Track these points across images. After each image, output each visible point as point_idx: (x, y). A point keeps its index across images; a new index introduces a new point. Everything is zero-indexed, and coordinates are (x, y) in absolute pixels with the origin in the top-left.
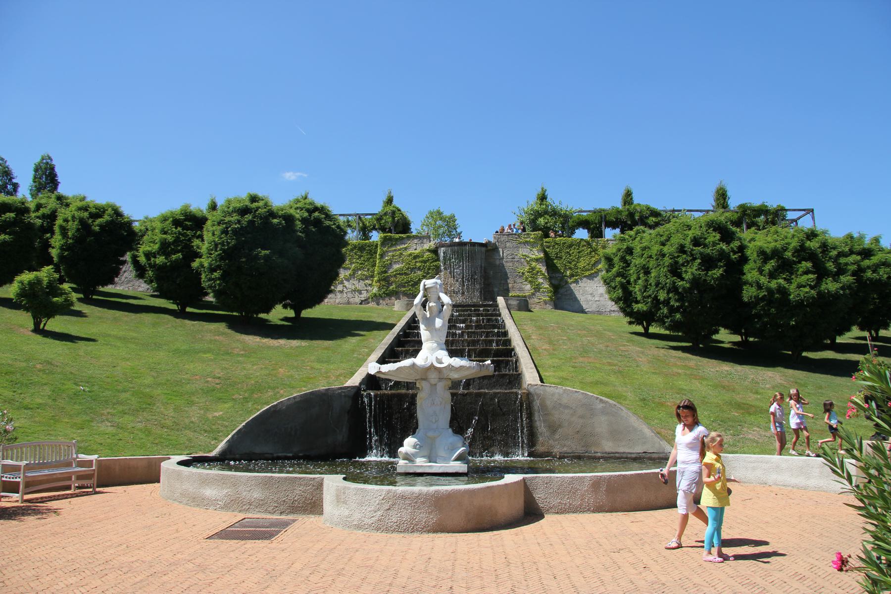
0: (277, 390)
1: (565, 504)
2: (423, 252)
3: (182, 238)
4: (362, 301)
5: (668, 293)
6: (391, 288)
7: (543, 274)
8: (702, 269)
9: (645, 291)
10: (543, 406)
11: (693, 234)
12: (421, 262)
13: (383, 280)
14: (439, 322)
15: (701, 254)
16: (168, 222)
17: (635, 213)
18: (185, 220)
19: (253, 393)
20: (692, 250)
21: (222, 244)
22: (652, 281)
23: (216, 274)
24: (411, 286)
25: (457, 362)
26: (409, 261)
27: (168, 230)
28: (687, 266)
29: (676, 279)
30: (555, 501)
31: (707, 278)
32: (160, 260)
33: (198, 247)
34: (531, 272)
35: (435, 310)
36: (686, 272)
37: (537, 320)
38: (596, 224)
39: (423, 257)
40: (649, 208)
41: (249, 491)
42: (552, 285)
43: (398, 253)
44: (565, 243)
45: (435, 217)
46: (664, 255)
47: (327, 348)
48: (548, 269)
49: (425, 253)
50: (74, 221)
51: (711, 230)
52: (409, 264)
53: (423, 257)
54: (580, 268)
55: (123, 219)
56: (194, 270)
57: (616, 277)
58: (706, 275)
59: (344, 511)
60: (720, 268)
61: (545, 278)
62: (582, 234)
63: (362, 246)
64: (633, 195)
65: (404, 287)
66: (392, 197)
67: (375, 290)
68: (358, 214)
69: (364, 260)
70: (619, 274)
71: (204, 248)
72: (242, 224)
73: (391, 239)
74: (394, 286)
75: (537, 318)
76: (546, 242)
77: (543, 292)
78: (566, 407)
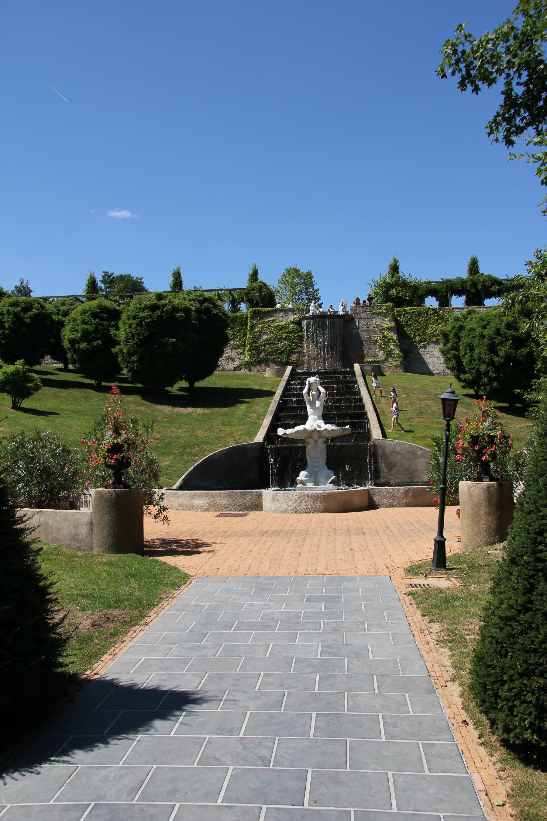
0: (201, 446)
1: (390, 503)
2: (288, 324)
3: (100, 328)
4: (235, 368)
5: (488, 366)
6: (261, 356)
7: (395, 342)
8: (513, 348)
9: (470, 364)
10: (384, 453)
11: (507, 320)
12: (287, 333)
13: (253, 350)
14: (318, 404)
15: (513, 336)
16: (87, 315)
17: (478, 284)
18: (101, 313)
19: (185, 449)
20: (506, 333)
21: (138, 334)
22: (475, 356)
23: (134, 358)
24: (279, 354)
25: (330, 427)
26: (277, 332)
27: (89, 321)
28: (501, 345)
29: (493, 356)
30: (384, 501)
31: (517, 355)
32: (83, 345)
33: (115, 335)
34: (384, 340)
35: (316, 396)
36: (501, 350)
37: (387, 385)
38: (443, 293)
39: (288, 329)
40: (491, 278)
41: (221, 500)
42: (402, 350)
43: (266, 325)
44: (414, 312)
45: (292, 275)
46: (484, 337)
47: (225, 414)
48: (398, 338)
49: (290, 324)
50: (9, 315)
51: (521, 317)
52: (276, 335)
53: (288, 329)
54: (428, 334)
55: (46, 311)
56: (113, 354)
57: (451, 351)
58: (516, 352)
59: (277, 505)
60: (527, 347)
61: (396, 345)
62: (431, 302)
63: (233, 319)
64: (479, 263)
65: (273, 355)
66: (257, 270)
67: (247, 358)
68: (228, 289)
69: (235, 331)
70: (453, 348)
71: (122, 335)
72: (154, 318)
73: (259, 313)
74: (264, 354)
75: (388, 383)
76: (397, 312)
77: (395, 357)
78: (399, 453)
